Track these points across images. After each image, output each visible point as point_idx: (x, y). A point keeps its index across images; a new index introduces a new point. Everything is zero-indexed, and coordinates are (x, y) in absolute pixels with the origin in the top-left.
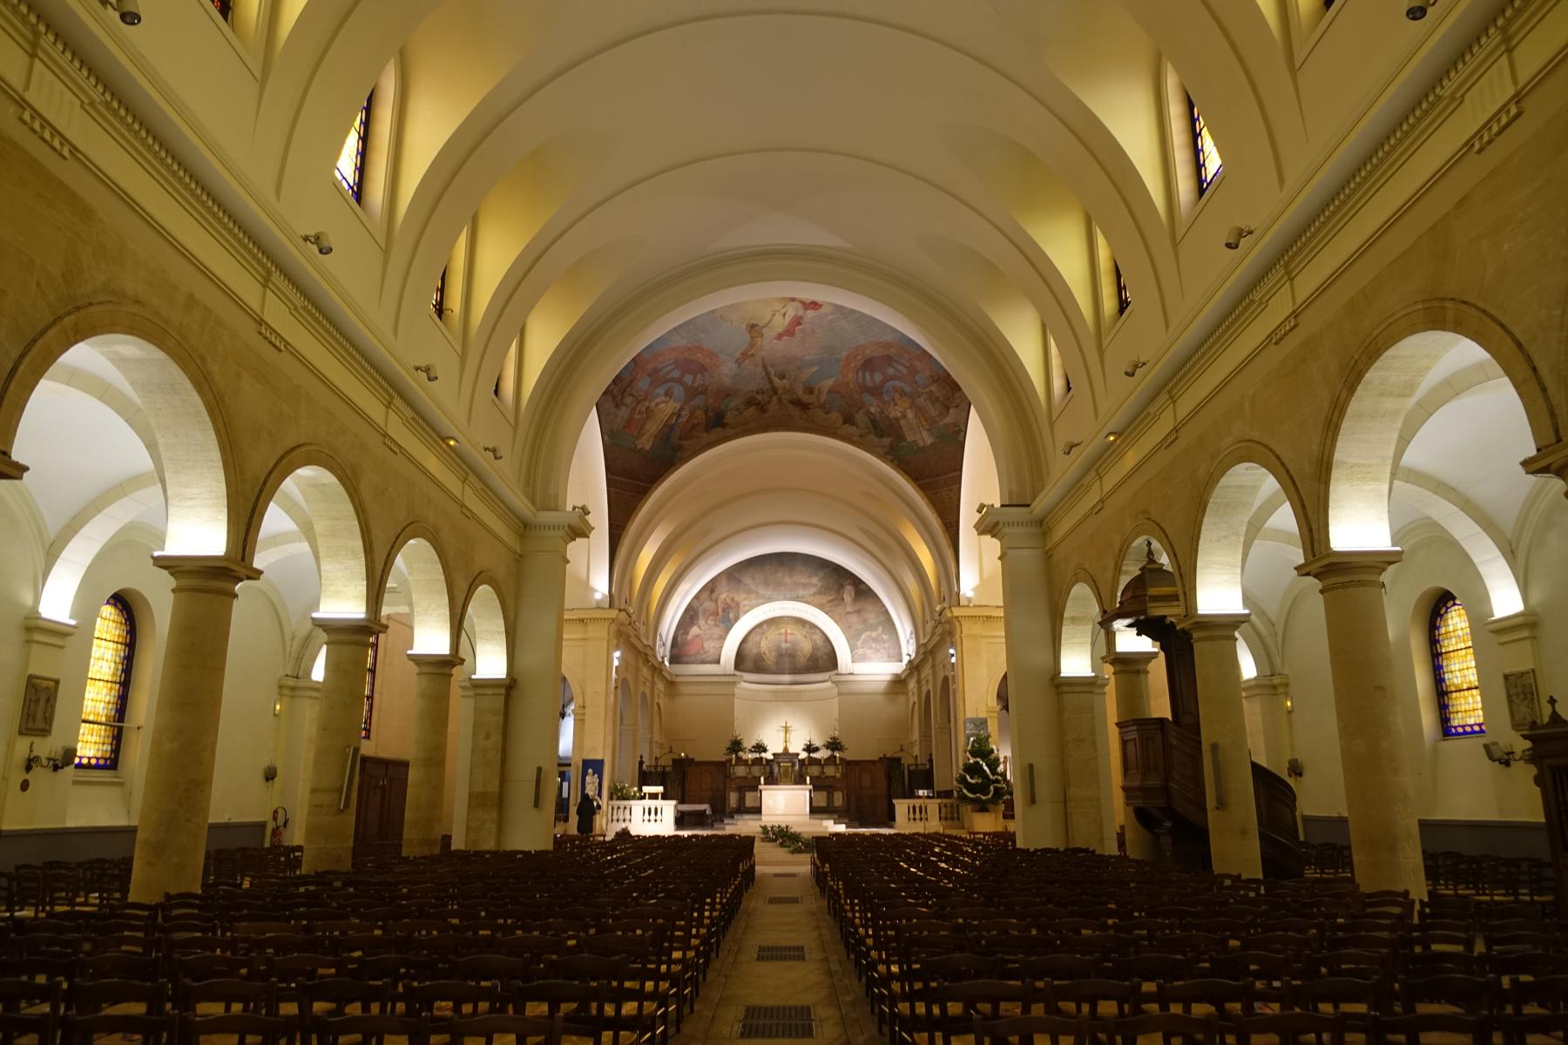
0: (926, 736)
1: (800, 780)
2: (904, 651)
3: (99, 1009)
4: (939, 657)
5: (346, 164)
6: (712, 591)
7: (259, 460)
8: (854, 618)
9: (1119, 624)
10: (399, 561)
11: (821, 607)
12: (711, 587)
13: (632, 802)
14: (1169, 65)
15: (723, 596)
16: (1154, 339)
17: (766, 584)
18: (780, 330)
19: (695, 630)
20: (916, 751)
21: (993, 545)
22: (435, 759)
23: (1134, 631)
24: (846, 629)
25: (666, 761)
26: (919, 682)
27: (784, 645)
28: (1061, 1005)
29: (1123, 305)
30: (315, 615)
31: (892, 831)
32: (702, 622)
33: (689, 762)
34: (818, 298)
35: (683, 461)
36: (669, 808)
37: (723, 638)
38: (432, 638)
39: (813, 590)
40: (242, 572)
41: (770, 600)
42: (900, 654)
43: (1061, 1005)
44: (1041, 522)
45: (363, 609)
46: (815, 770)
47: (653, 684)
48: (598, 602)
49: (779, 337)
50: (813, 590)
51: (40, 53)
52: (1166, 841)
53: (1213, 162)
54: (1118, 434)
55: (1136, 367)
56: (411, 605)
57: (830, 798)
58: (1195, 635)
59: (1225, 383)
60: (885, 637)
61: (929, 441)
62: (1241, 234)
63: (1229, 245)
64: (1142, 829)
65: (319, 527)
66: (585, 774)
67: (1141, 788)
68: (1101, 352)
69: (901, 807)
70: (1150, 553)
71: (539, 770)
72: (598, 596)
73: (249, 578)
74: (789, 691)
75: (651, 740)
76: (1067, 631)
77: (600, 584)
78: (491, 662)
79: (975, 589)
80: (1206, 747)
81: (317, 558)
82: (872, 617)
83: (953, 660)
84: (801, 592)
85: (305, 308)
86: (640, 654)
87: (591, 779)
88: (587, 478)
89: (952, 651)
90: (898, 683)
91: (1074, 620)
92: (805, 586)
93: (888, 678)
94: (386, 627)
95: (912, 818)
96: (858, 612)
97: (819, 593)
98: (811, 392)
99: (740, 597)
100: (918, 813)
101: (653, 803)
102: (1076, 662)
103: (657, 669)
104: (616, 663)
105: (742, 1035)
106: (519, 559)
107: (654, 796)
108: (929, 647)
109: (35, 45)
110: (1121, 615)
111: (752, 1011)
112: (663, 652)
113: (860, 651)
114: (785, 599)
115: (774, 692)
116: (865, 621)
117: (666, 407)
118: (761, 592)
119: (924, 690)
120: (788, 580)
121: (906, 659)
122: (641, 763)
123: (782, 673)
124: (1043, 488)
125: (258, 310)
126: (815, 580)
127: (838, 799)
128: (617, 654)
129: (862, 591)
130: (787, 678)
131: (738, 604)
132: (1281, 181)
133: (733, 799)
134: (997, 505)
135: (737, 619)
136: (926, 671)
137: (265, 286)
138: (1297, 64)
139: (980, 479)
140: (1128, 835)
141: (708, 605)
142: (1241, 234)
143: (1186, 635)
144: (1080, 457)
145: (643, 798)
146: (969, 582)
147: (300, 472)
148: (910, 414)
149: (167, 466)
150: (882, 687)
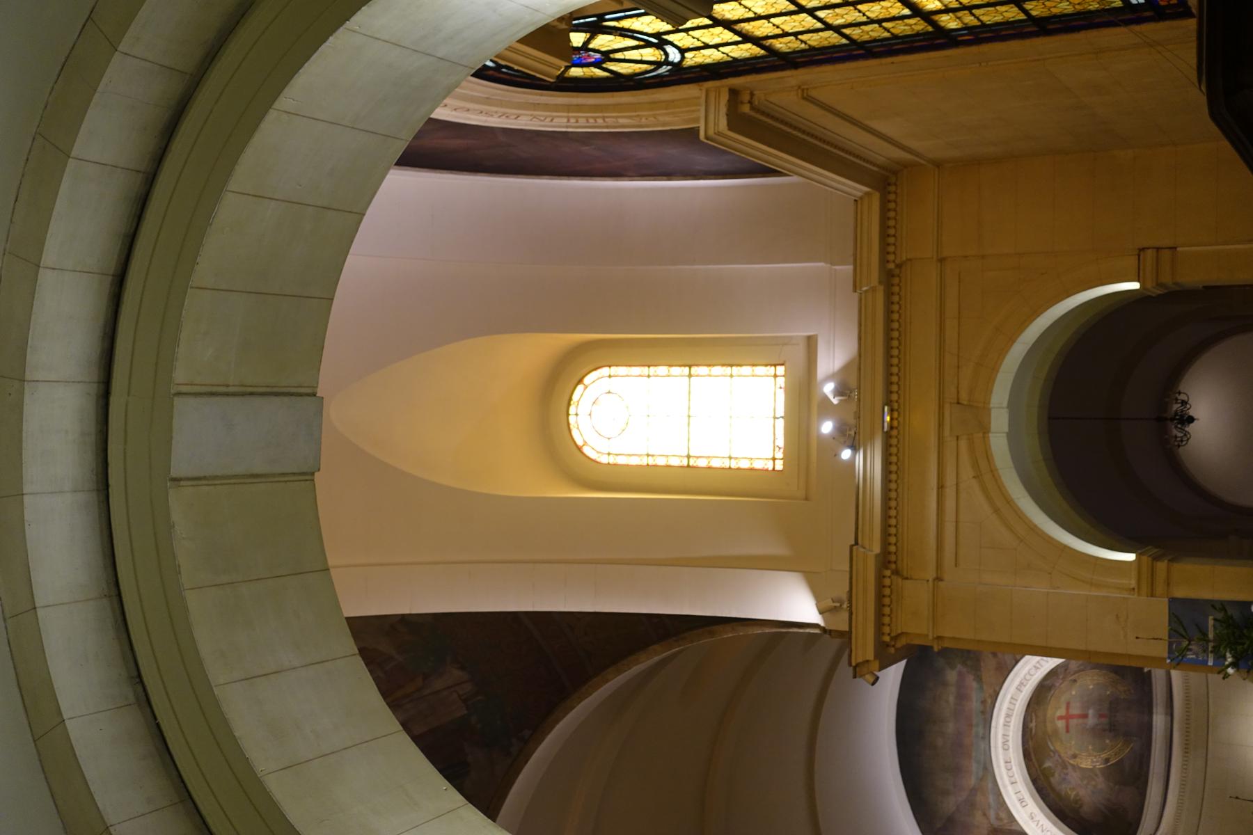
17: (957, 770)
27: (1091, 721)
34: (454, 113)
50: (971, 682)
74: (1187, 720)
84: (975, 704)
92: (962, 697)
114: (986, 737)
115: (1186, 750)
118: (973, 781)
120: (950, 727)
123: (1149, 727)
126: (952, 676)
130: (1159, 720)
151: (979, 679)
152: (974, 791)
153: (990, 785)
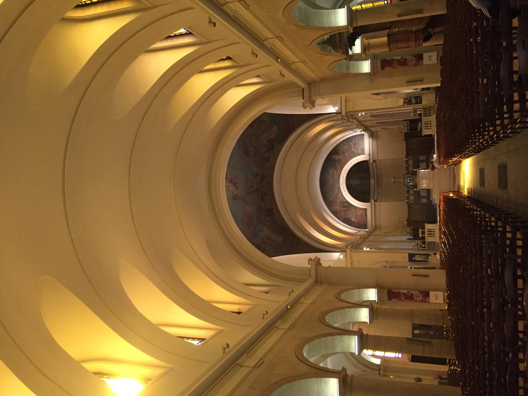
0: (395, 123)
1: (415, 174)
2: (359, 133)
4: (362, 119)
5: (195, 342)
6: (336, 212)
7: (303, 368)
8: (346, 154)
9: (350, 53)
10: (336, 325)
11: (342, 168)
12: (335, 213)
13: (426, 241)
14: (66, 15)
15: (338, 208)
16: (244, 47)
18: (234, 188)
19: (353, 219)
20: (402, 126)
21: (319, 101)
22: (411, 315)
23: (353, 47)
25: (408, 229)
26: (372, 127)
29: (229, 58)
30: (357, 354)
31: (436, 136)
32: (349, 216)
33: (408, 220)
35: (286, 224)
36: (428, 226)
37: (356, 207)
38: (364, 315)
39: (335, 172)
40: (343, 373)
41: (339, 189)
42: (360, 135)
44: (309, 84)
45: (354, 336)
46: (411, 168)
47: (376, 235)
48: (344, 257)
49: (237, 188)
50: (335, 172)
52: (436, 30)
53: (183, 31)
54: (278, 58)
55: (254, 54)
56: (350, 323)
57: (422, 161)
58: (355, 25)
59: (262, 22)
60: (354, 141)
61: (275, 128)
62: (210, 22)
63: (215, 26)
64: (433, 38)
65: (323, 352)
66: (415, 261)
67: (415, 41)
68: (248, 65)
69: (425, 132)
70: (323, 43)
71: (413, 275)
72: (341, 257)
73: (346, 371)
75: (399, 235)
76: (352, 71)
77: (336, 255)
78: (372, 294)
79: (334, 107)
80: (399, 19)
81: (335, 353)
82: (345, 147)
83: (363, 114)
84: (336, 176)
85: (248, 354)
86: (364, 240)
87: (417, 258)
88: (298, 260)
89: (360, 114)
90: (372, 135)
91: (348, 69)
92: (333, 175)
93: (371, 140)
94: (360, 329)
95: (430, 128)
96: (343, 153)
97: (336, 169)
98: (258, 175)
99: (339, 201)
100: (428, 125)
101: (426, 233)
102: (366, 67)
103: (370, 234)
104: (368, 249)
105: (507, 189)
106: (331, 284)
107: (423, 233)
108: (358, 123)
109: (239, 365)
110: (347, 52)
111: (500, 187)
112: (363, 232)
113: (360, 151)
116: (347, 150)
117: (266, 231)
119: (370, 118)
120: (331, 182)
121: (363, 132)
122: (409, 239)
124: (296, 83)
125: (250, 368)
126: (331, 171)
127: (422, 158)
128: (365, 249)
129: (336, 151)
131: (341, 202)
132: (192, 8)
133: (424, 201)
134: (303, 101)
135: (348, 202)
136: (368, 124)
137: (242, 366)
138: (152, 6)
139: (295, 108)
140: (419, 354)
141: (342, 214)
142: (210, 22)
143: (355, 28)
144: (285, 72)
145: (424, 237)
146: (332, 109)
147: (305, 355)
148: (265, 136)
149: (331, 351)
150: (375, 142)
151: (337, 171)
152: (337, 194)
153: (340, 195)
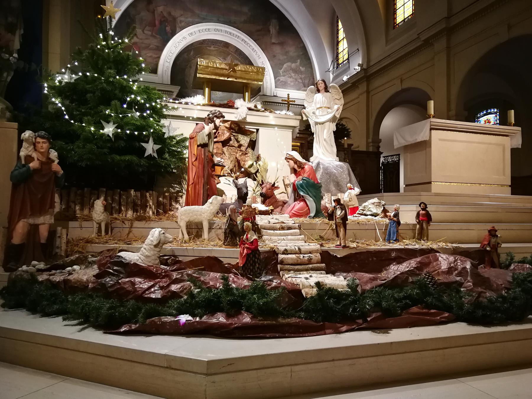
3: (353, 287)
8: (277, 49)
15: (160, 9)
24: (271, 58)
28: (357, 321)
37: (160, 49)
43: (357, 321)
50: (243, 18)
51: (297, 231)
60: (303, 69)
82: (292, 50)
84: (233, 18)
96: (281, 44)
99: (177, 13)
114: (219, 21)
118: (197, 11)
126: (245, 9)
129: (287, 28)
131: (175, 19)
135: (173, 34)
